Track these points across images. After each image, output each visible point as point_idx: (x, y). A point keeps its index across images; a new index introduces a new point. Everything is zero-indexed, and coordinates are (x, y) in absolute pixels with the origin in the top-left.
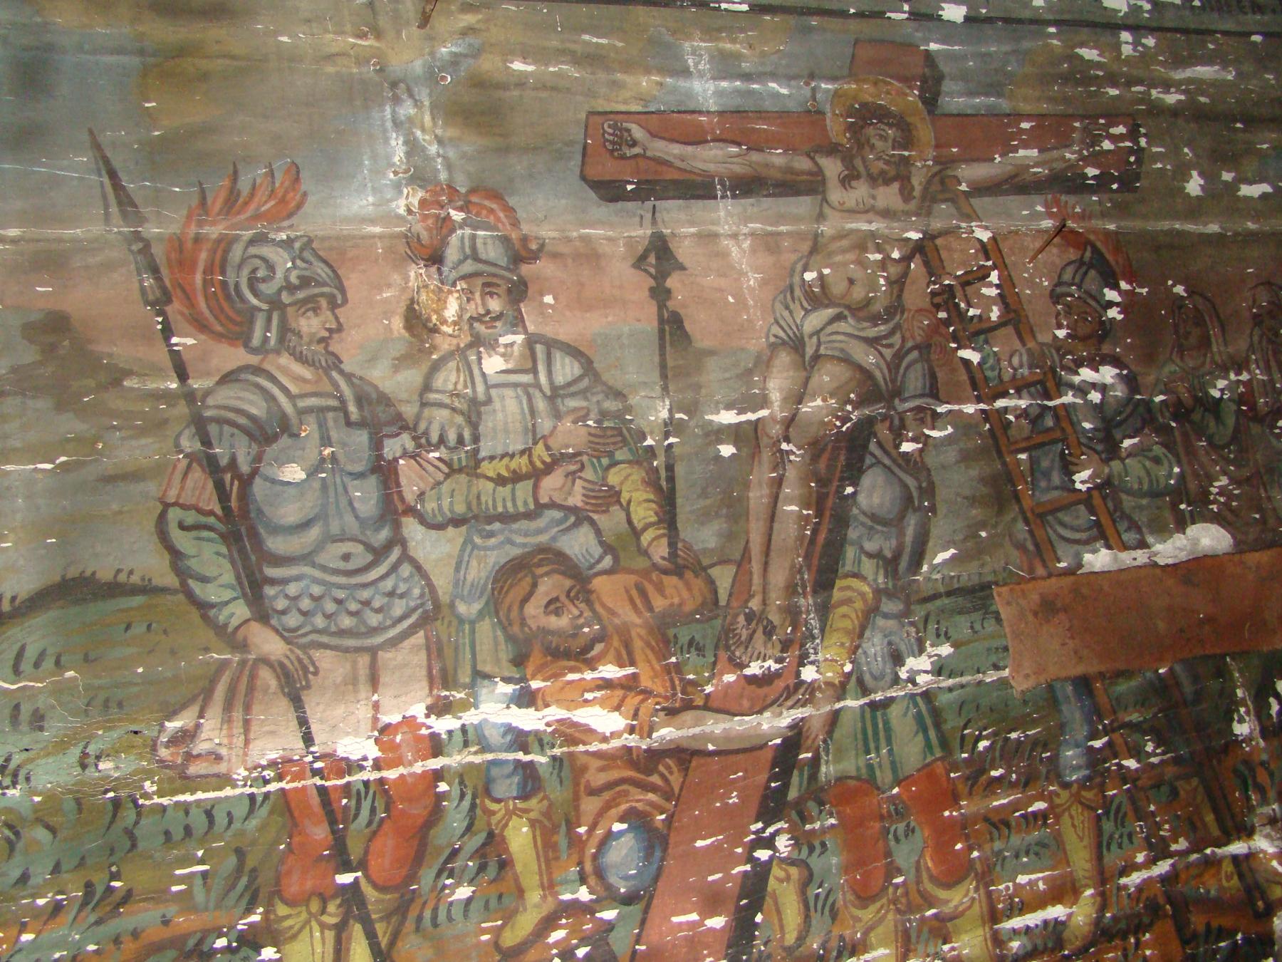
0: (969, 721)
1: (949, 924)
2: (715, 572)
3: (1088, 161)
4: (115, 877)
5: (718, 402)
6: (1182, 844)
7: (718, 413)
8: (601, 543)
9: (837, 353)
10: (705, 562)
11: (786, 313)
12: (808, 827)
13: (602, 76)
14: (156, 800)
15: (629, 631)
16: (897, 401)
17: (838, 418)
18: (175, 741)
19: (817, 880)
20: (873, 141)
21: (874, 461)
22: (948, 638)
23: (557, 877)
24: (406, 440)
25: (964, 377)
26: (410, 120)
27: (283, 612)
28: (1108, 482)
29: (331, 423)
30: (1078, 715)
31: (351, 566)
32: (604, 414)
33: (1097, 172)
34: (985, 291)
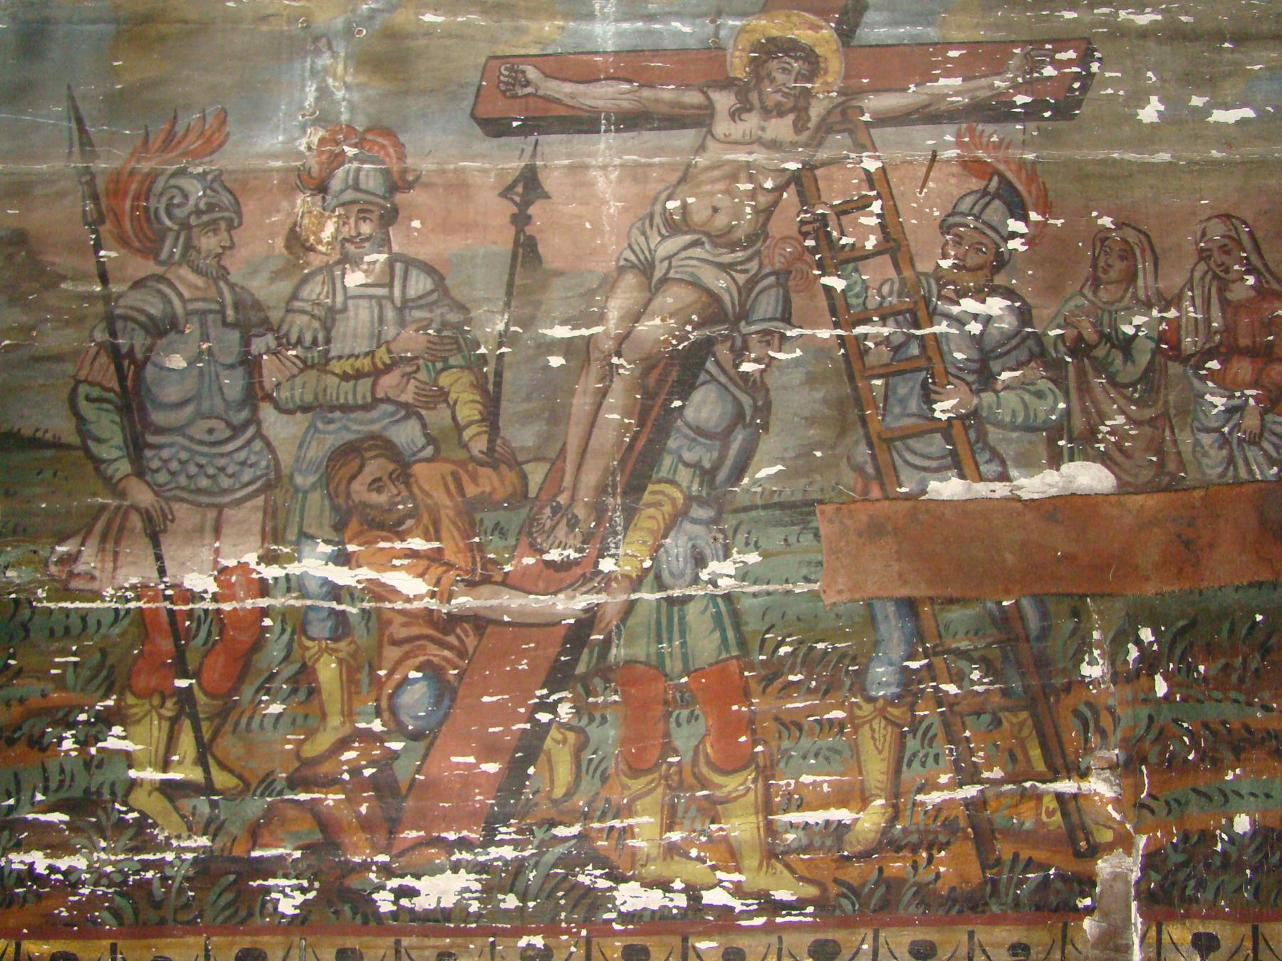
0: (773, 626)
1: (719, 807)
2: (528, 468)
3: (1017, 88)
4: (12, 657)
5: (554, 318)
6: (997, 773)
7: (552, 328)
8: (426, 435)
9: (686, 277)
10: (521, 458)
11: (641, 239)
12: (591, 700)
13: (506, 23)
14: (45, 604)
15: (438, 511)
16: (743, 323)
17: (674, 337)
18: (62, 561)
19: (591, 747)
20: (774, 74)
21: (708, 378)
22: (757, 547)
23: (358, 707)
24: (270, 340)
25: (823, 303)
26: (325, 69)
27: (157, 471)
28: (975, 413)
29: (210, 323)
30: (896, 635)
31: (212, 439)
32: (445, 325)
33: (1028, 99)
34: (863, 220)
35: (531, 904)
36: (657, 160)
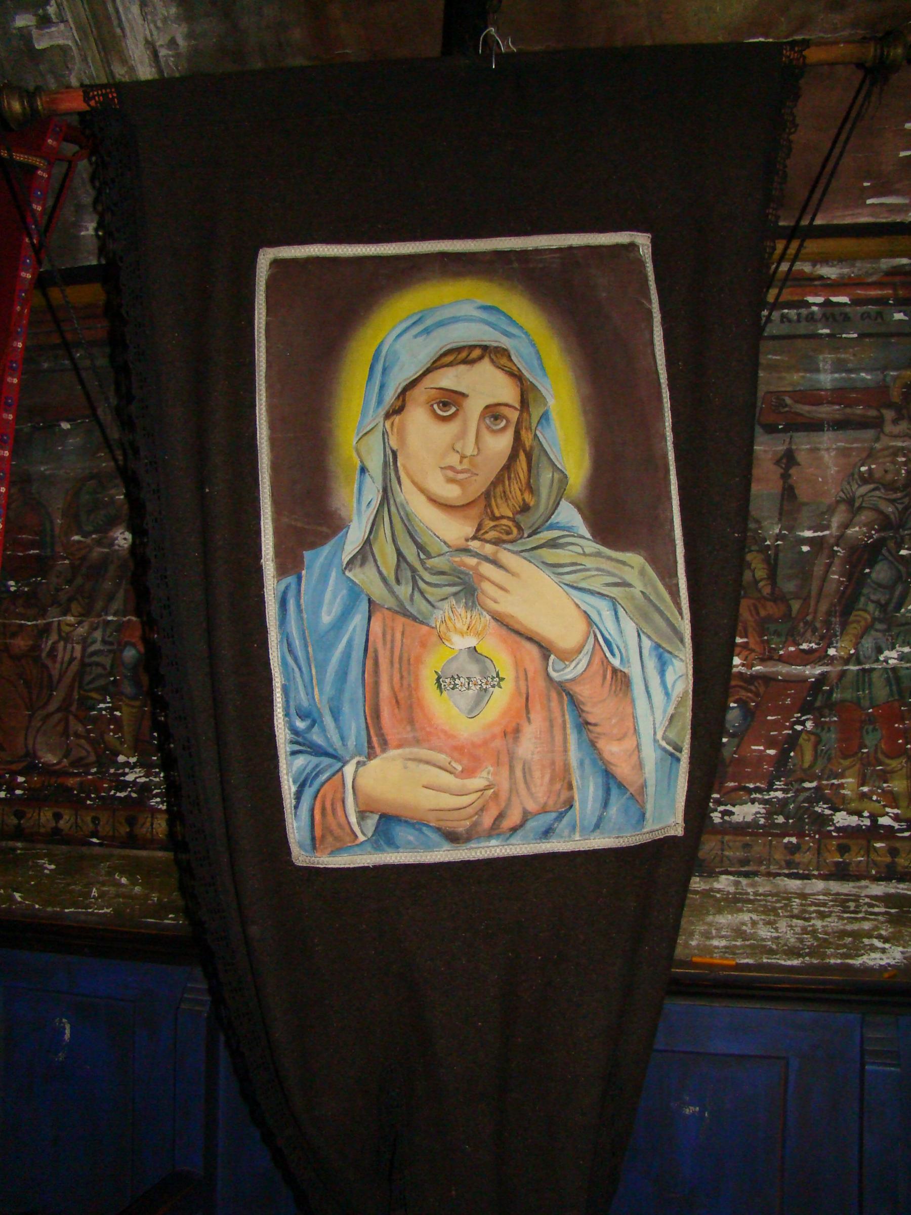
2: (792, 602)
11: (848, 487)
13: (775, 375)
35: (791, 821)
36: (855, 445)
